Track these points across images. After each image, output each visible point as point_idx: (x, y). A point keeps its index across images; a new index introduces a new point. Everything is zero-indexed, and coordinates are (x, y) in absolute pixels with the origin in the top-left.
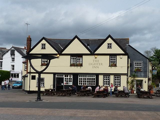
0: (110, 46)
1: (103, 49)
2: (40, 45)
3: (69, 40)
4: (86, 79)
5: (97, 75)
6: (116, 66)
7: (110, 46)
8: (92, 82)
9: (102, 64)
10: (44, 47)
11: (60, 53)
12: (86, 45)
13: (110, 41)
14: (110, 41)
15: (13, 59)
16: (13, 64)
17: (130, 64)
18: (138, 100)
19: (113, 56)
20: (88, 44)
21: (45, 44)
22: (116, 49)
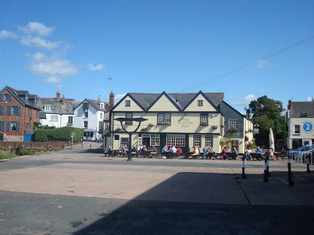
0: (200, 103)
1: (193, 107)
2: (124, 103)
3: (193, 94)
4: (154, 139)
5: (187, 135)
6: (296, 126)
7: (200, 103)
8: (179, 142)
9: (192, 123)
10: (128, 104)
11: (146, 111)
12: (175, 101)
13: (200, 97)
14: (200, 97)
15: (87, 116)
16: (86, 120)
17: (225, 122)
18: (252, 170)
19: (205, 114)
20: (177, 100)
21: (129, 101)
22: (207, 107)
